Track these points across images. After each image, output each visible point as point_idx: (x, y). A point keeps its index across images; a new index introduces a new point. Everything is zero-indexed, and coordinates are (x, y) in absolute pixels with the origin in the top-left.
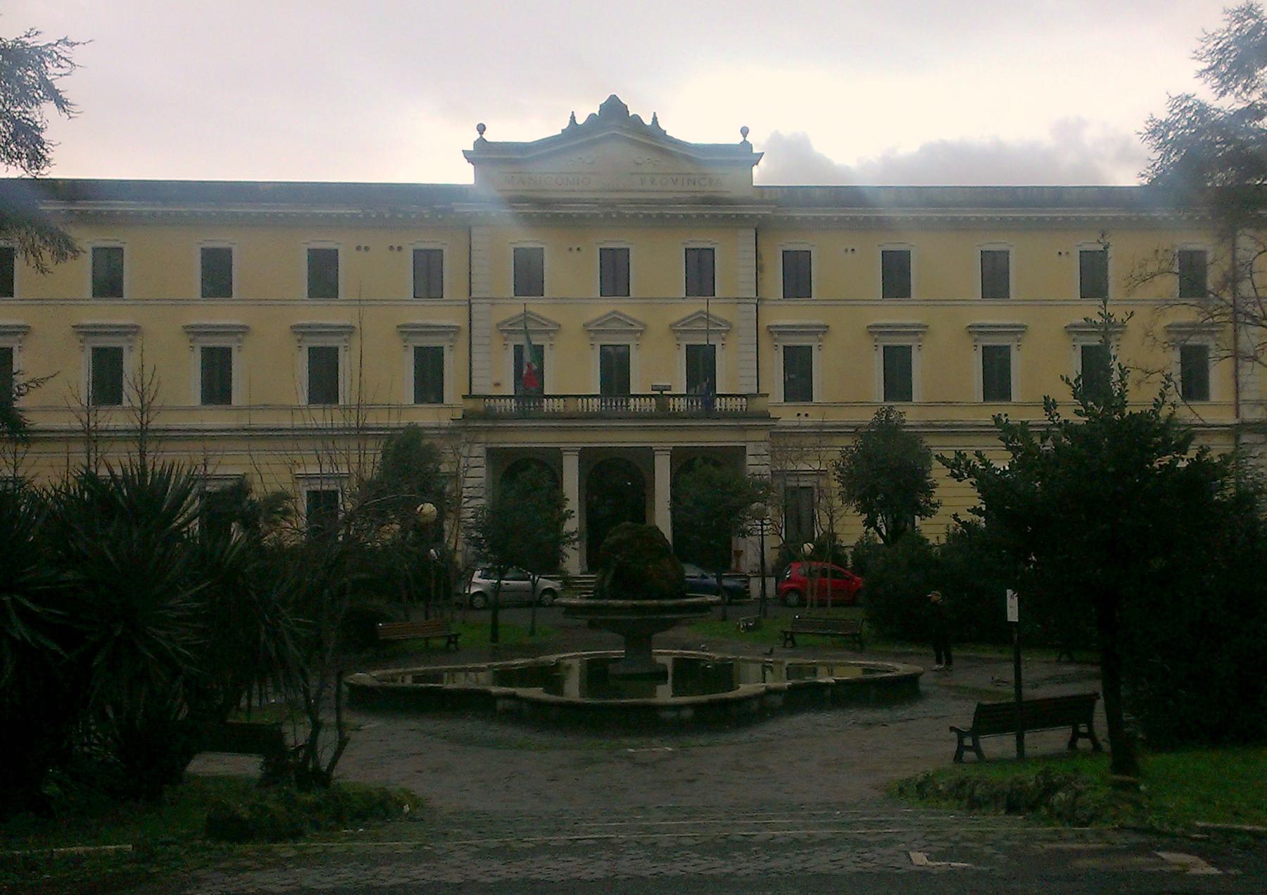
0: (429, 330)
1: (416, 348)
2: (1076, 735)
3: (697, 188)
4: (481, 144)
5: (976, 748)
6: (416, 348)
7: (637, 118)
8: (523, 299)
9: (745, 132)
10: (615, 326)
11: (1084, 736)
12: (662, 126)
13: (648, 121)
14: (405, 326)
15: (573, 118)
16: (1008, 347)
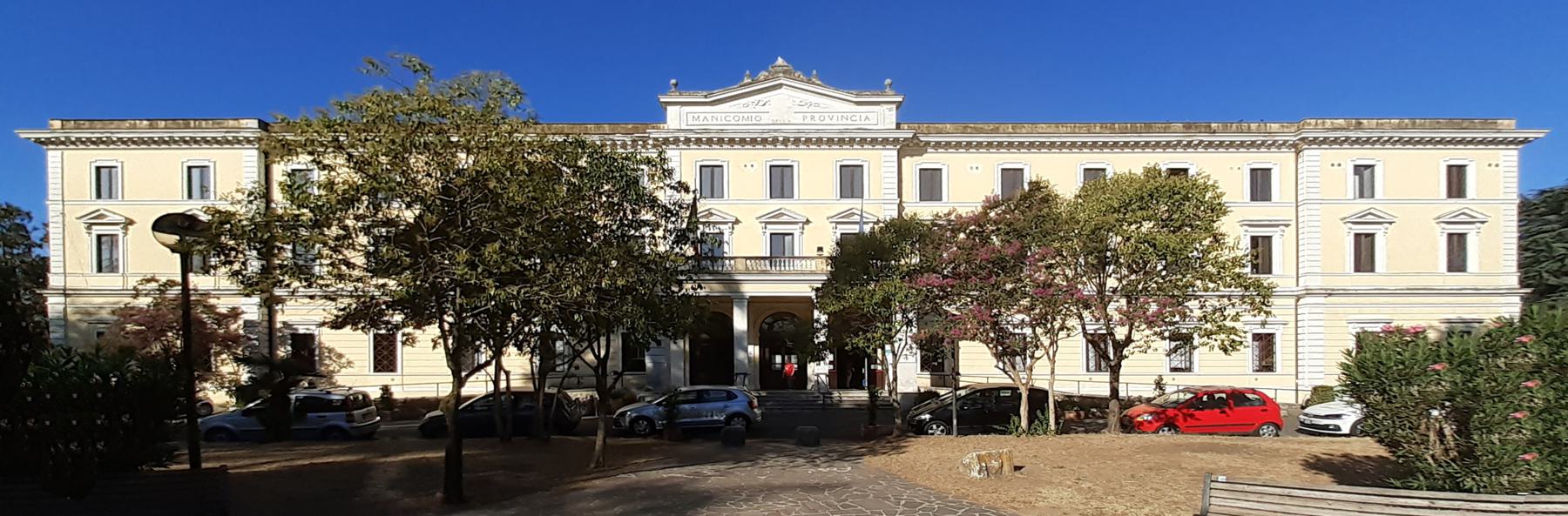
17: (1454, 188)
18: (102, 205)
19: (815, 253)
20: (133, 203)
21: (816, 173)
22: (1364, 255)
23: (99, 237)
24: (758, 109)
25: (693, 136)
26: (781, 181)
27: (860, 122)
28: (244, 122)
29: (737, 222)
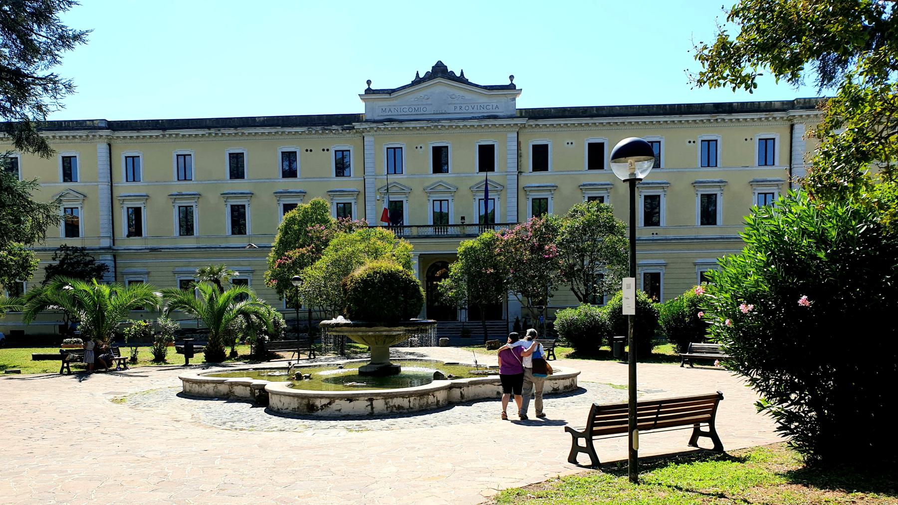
0: (540, 188)
1: (232, 206)
2: (697, 433)
3: (485, 110)
4: (369, 91)
5: (590, 450)
6: (232, 206)
7: (452, 72)
8: (484, 174)
9: (512, 77)
10: (441, 189)
11: (705, 434)
12: (466, 76)
13: (458, 74)
14: (584, 185)
15: (417, 73)
16: (402, 201)
18: (393, 178)
19: (459, 222)
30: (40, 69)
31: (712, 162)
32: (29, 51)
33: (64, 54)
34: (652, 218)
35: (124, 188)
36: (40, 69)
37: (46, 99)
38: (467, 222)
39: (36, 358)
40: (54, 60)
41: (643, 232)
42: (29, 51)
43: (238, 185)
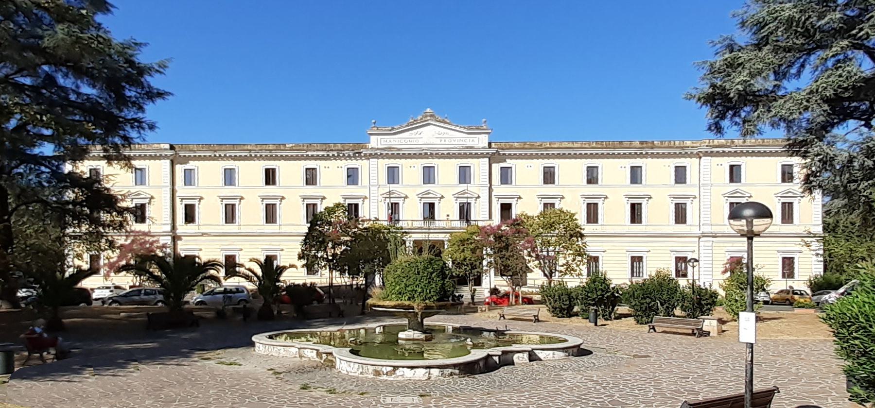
17: (427, 178)
18: (393, 187)
19: (446, 218)
20: (564, 186)
21: (447, 170)
22: (680, 215)
23: (267, 205)
24: (417, 136)
25: (379, 152)
26: (429, 175)
27: (469, 143)
28: (162, 146)
29: (442, 197)
30: (130, 113)
31: (432, 181)
32: (122, 101)
33: (149, 107)
34: (190, 217)
35: (500, 190)
36: (130, 113)
37: (133, 134)
38: (450, 218)
39: (566, 341)
40: (141, 109)
41: (182, 227)
42: (122, 101)
43: (271, 190)
